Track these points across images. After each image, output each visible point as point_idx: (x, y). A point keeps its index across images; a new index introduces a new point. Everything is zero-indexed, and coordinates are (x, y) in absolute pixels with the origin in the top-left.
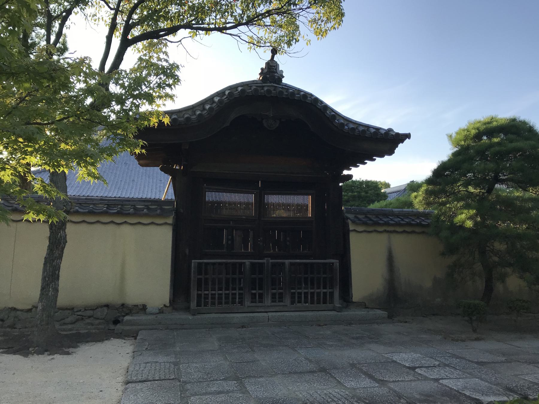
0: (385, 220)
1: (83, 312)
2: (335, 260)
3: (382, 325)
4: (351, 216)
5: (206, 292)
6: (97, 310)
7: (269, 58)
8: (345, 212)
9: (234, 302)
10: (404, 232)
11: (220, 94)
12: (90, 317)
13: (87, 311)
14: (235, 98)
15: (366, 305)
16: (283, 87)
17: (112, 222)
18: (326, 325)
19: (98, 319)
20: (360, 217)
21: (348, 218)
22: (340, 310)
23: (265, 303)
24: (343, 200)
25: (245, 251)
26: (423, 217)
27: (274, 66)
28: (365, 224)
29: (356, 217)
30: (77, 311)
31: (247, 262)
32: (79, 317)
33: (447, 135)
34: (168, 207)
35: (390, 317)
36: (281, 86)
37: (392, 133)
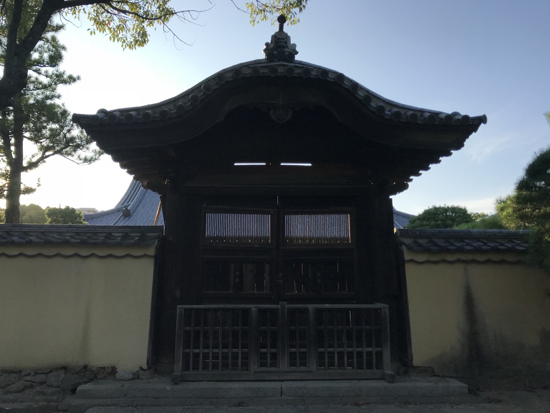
0: (458, 244)
1: (33, 376)
2: (384, 305)
3: (458, 406)
4: (408, 241)
5: (197, 351)
6: (51, 373)
7: (277, 29)
8: (398, 235)
9: (331, 364)
10: (488, 261)
11: (211, 80)
12: (42, 383)
13: (38, 376)
14: (227, 82)
15: (434, 372)
16: (297, 65)
17: (76, 255)
18: (368, 404)
19: (51, 386)
20: (421, 241)
21: (402, 244)
22: (392, 379)
23: (279, 367)
24: (75, 127)
25: (258, 293)
26: (517, 240)
27: (283, 39)
28: (426, 250)
29: (415, 242)
30: (26, 375)
31: (253, 307)
32: (28, 382)
33: (544, 114)
34: (153, 234)
35: (473, 391)
36: (294, 65)
37: (457, 117)
